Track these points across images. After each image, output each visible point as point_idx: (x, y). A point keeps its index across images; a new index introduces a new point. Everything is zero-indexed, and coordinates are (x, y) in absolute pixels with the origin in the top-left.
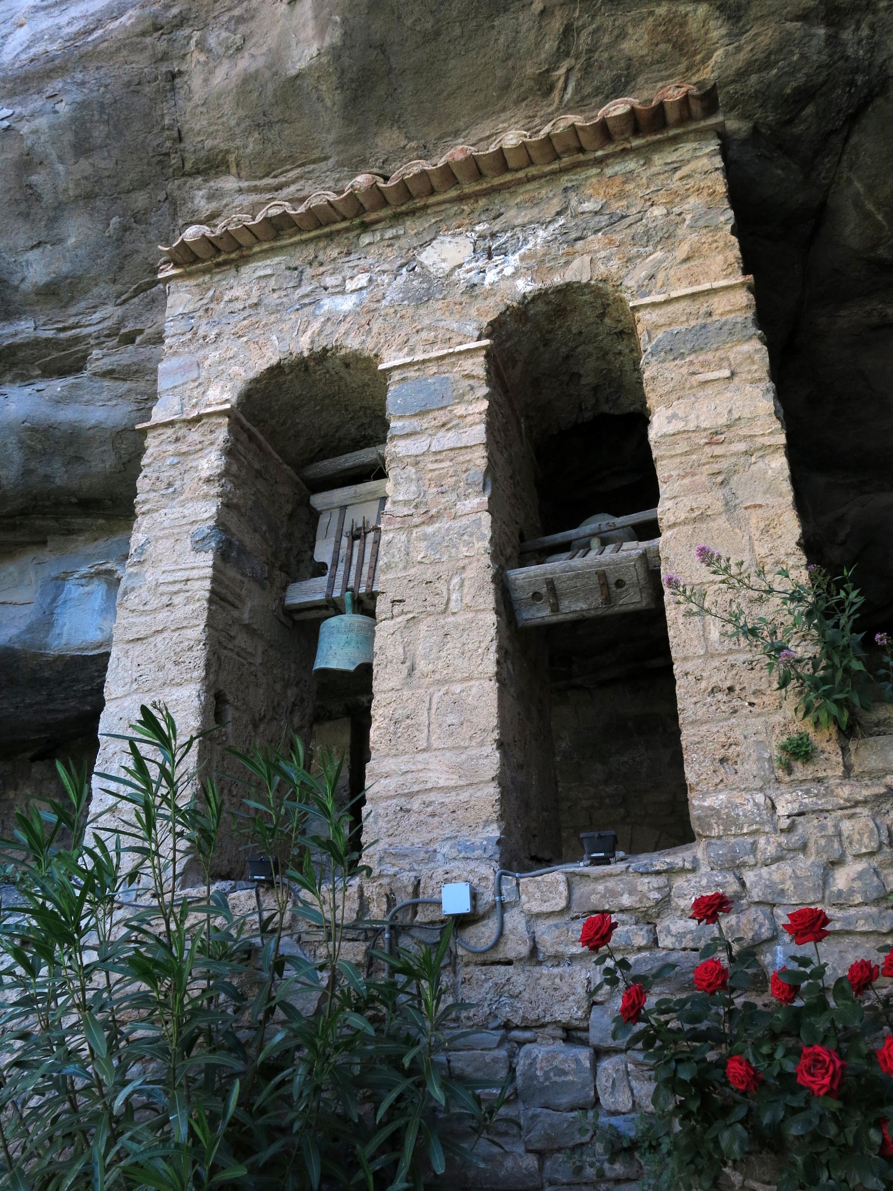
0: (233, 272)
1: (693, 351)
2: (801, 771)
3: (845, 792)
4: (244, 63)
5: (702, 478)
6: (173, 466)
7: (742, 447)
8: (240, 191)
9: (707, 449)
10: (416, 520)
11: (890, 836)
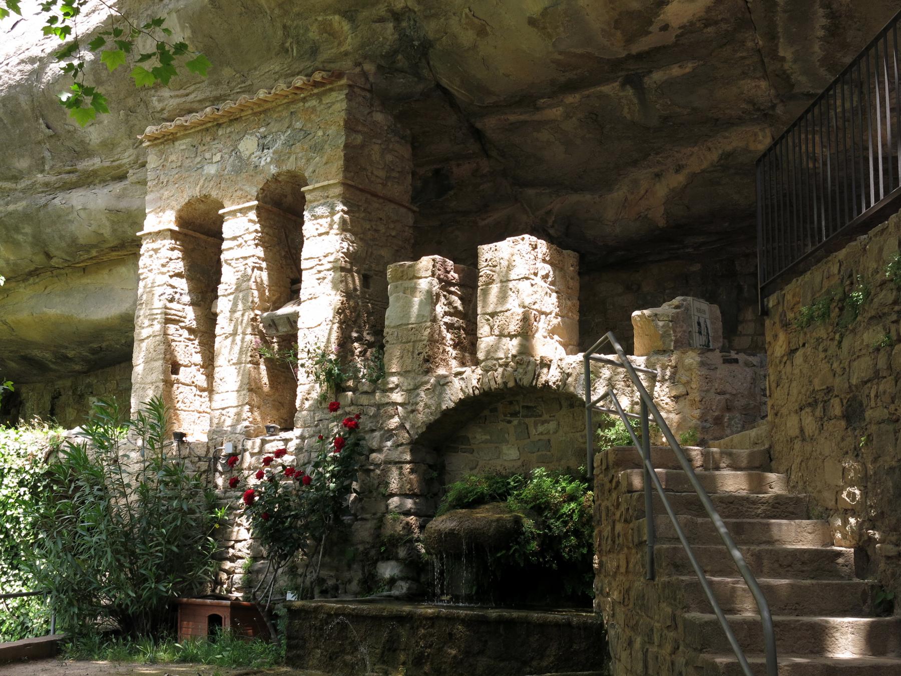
11: (898, 334)
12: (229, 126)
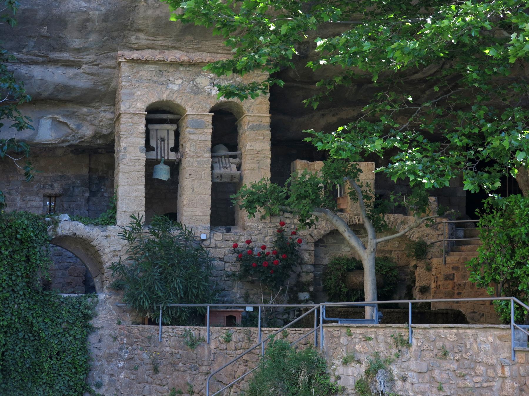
0: (142, 65)
1: (257, 130)
2: (263, 221)
3: (270, 225)
4: (158, 12)
5: (255, 161)
6: (131, 126)
7: (263, 156)
8: (145, 39)
9: (257, 155)
10: (195, 157)
12: (189, 67)
